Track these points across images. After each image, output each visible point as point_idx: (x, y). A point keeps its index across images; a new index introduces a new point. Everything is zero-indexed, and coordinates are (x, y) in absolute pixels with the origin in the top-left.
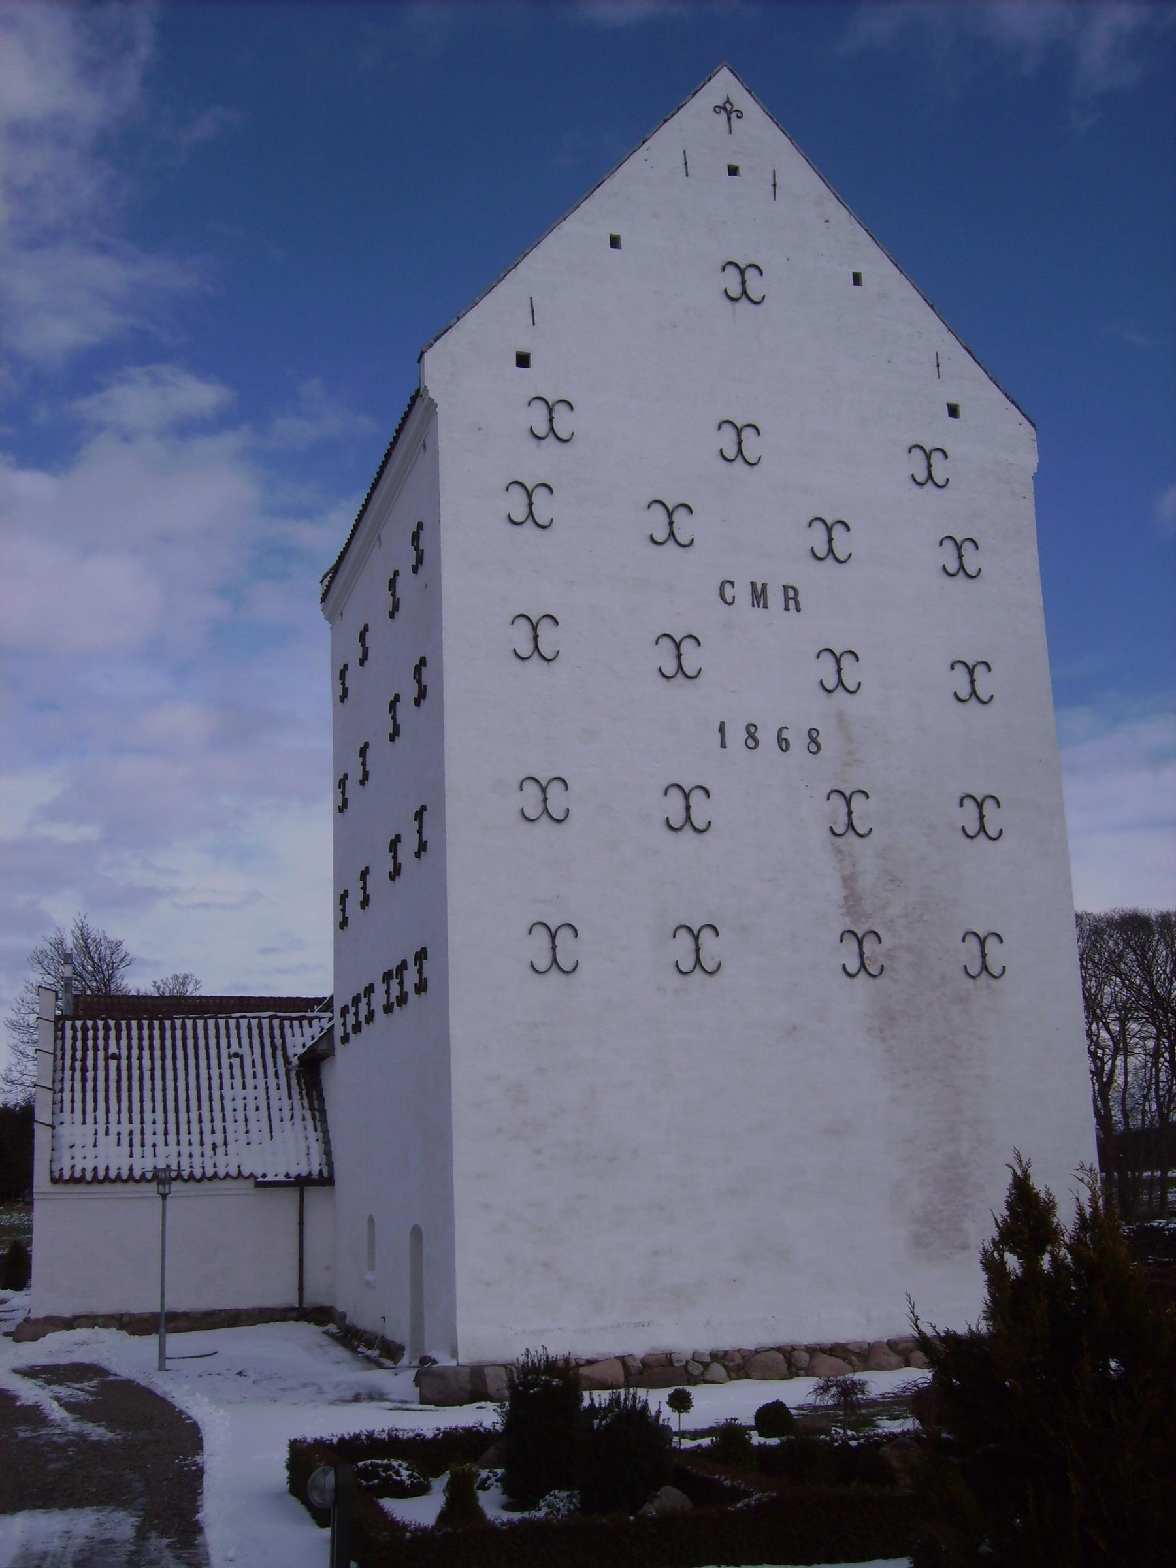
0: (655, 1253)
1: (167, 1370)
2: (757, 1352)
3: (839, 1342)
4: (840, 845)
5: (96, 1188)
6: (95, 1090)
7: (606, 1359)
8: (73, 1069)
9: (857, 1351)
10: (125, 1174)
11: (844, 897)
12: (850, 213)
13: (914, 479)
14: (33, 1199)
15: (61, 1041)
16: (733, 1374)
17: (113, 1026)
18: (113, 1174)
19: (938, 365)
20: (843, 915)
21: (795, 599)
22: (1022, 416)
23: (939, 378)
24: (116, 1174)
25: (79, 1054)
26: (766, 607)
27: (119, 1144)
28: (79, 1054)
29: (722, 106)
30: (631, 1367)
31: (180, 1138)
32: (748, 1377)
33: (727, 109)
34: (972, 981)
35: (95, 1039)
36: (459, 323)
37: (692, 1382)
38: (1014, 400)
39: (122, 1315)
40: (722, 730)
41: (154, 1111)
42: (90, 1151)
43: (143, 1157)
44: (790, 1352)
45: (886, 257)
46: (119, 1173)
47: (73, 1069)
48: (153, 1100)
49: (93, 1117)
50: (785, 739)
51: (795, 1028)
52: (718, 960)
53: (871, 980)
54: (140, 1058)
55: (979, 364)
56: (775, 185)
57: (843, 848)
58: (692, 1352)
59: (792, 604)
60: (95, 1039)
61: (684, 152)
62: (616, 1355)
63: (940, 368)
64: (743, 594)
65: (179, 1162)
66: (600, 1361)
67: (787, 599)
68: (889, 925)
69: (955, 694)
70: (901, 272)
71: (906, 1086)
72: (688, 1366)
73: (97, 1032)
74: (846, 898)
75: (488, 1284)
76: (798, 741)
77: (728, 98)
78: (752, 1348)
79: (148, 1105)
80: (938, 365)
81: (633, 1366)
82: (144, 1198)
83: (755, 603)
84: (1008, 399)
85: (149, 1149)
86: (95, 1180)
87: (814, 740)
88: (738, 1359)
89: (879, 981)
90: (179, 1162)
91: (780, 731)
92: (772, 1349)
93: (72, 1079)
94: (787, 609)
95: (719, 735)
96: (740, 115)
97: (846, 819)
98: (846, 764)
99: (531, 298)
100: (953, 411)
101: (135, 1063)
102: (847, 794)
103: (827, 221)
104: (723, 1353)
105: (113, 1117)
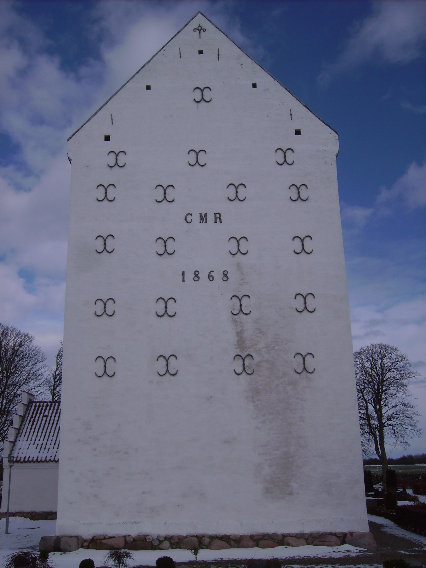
0: (143, 493)
1: (9, 533)
2: (187, 537)
3: (227, 534)
4: (236, 319)
5: (24, 464)
6: (35, 429)
7: (118, 537)
8: (30, 421)
9: (234, 538)
10: (43, 460)
11: (237, 341)
12: (252, 60)
13: (278, 163)
14: (3, 468)
15: (29, 411)
16: (173, 546)
17: (49, 405)
18: (30, 459)
19: (291, 115)
20: (236, 348)
21: (220, 218)
22: (332, 130)
23: (291, 120)
24: (32, 459)
25: (34, 416)
26: (206, 222)
27: (36, 448)
28: (34, 416)
29: (197, 28)
30: (127, 541)
31: (59, 446)
32: (180, 548)
33: (200, 29)
34: (298, 375)
35: (42, 409)
36: (82, 128)
37: (153, 548)
38: (328, 124)
39: (33, 512)
40: (183, 274)
41: (53, 436)
42: (26, 450)
43: (43, 453)
44: (201, 538)
45: (268, 75)
46: (42, 459)
47: (30, 421)
48: (54, 432)
49: (31, 438)
50: (211, 276)
51: (211, 397)
52: (177, 369)
53: (248, 376)
54: (55, 416)
55: (311, 111)
56: (218, 55)
57: (238, 320)
58: (157, 535)
59: (218, 220)
60: (42, 409)
61: (180, 49)
62: (123, 535)
63: (292, 116)
64: (196, 218)
65: (56, 455)
66: (116, 537)
67: (216, 218)
68: (258, 352)
69: (294, 251)
70: (275, 79)
71: (264, 422)
72: (153, 541)
73: (43, 407)
74: (238, 341)
75: (71, 503)
76: (218, 276)
77: (200, 25)
78: (185, 535)
79: (52, 433)
80: (291, 115)
81: (128, 540)
82: (25, 468)
83: (201, 222)
84: (325, 124)
85: (47, 450)
86: (24, 461)
87: (225, 276)
88: (177, 540)
89: (252, 376)
90: (56, 455)
91: (210, 273)
92: (194, 536)
93: (29, 425)
94: (216, 222)
95: (182, 276)
96: (204, 30)
97: (239, 307)
98: (240, 285)
99: (112, 114)
100: (298, 132)
101: (53, 418)
102: (240, 297)
103: (242, 65)
104: (170, 536)
105: (38, 438)
